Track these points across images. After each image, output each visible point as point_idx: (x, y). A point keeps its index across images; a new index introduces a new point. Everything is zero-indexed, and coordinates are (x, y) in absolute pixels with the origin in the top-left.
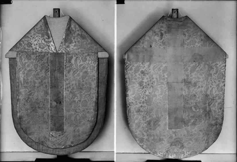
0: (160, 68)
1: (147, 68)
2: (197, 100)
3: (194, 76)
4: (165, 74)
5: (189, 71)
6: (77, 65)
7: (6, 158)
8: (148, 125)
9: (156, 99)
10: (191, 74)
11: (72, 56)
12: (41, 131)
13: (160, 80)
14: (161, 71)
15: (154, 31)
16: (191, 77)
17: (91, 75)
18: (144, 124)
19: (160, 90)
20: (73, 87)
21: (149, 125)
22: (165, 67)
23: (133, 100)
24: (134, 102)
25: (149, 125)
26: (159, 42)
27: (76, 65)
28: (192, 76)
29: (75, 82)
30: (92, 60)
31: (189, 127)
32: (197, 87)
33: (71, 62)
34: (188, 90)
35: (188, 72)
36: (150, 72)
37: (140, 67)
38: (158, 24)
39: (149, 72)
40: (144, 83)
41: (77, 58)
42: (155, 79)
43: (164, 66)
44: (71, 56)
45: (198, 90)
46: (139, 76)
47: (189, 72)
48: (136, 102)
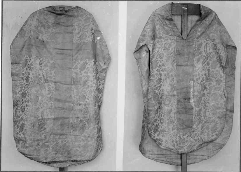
0: (46, 64)
1: (33, 62)
2: (86, 102)
3: (83, 74)
4: (53, 72)
5: (78, 69)
6: (207, 52)
7: (2, 170)
8: (32, 127)
9: (204, 98)
10: (81, 73)
11: (202, 42)
12: (167, 132)
13: (209, 76)
14: (48, 68)
15: (41, 21)
16: (81, 76)
17: (90, 67)
18: (35, 129)
19: (47, 89)
20: (202, 78)
21: (34, 127)
22: (53, 63)
23: (20, 98)
24: (21, 100)
25: (34, 127)
26: (46, 35)
27: (206, 52)
28: (81, 74)
29: (205, 72)
30: (222, 50)
31: (77, 131)
32: (87, 86)
33: (200, 50)
34: (76, 91)
35: (77, 70)
36: (36, 66)
37: (158, 61)
38: (196, 17)
39: (35, 67)
40: (29, 79)
41: (207, 44)
42: (41, 76)
43: (51, 62)
44: (201, 42)
45: (87, 90)
46: (157, 72)
47: (79, 70)
48: (23, 100)
